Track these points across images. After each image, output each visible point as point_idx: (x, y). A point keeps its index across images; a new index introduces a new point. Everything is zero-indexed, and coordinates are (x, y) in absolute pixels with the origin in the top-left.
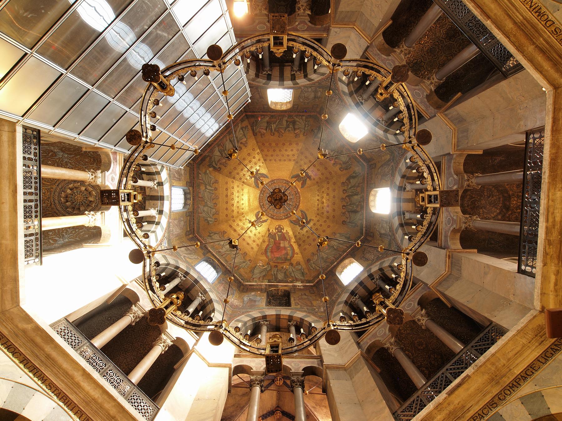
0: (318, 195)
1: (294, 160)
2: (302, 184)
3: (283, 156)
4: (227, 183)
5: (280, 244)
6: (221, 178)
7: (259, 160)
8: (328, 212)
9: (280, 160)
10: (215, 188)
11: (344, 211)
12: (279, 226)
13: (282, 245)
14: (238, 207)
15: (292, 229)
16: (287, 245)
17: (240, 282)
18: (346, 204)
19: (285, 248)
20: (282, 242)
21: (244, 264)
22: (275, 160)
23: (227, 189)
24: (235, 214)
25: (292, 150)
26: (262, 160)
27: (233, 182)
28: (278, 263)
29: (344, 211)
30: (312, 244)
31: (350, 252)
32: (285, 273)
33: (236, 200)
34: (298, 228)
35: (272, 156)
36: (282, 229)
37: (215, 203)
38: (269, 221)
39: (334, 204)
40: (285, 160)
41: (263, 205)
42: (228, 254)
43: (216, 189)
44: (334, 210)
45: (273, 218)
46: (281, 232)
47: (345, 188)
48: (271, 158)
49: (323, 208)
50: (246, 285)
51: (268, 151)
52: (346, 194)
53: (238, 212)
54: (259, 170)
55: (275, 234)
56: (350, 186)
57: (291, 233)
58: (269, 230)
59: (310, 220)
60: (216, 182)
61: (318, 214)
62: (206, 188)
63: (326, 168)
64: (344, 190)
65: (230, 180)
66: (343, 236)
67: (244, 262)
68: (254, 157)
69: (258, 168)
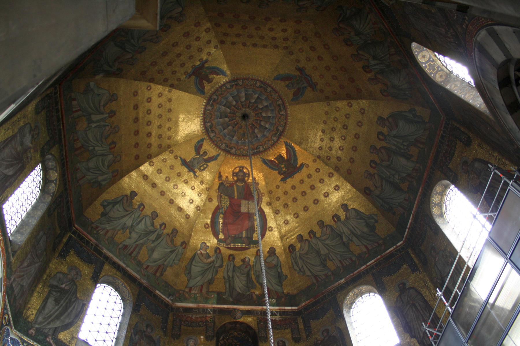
0: (325, 122)
1: (286, 48)
2: (295, 94)
3: (262, 38)
4: (136, 94)
5: (240, 206)
6: (123, 87)
7: (209, 42)
8: (339, 159)
9: (255, 45)
10: (112, 111)
11: (371, 171)
12: (241, 168)
13: (244, 209)
14: (160, 137)
15: (266, 177)
16: (253, 208)
17: (167, 305)
18: (378, 161)
19: (249, 216)
20: (244, 202)
21: (173, 256)
22: (244, 45)
23: (136, 107)
24: (154, 140)
25: (284, 31)
26: (215, 42)
27: (149, 88)
28: (235, 249)
29: (371, 171)
30: (301, 217)
31: (372, 267)
32: (248, 275)
33: (154, 130)
34: (277, 177)
35: (238, 35)
36: (245, 174)
37: (114, 143)
38: (220, 158)
39: (355, 149)
40: (265, 46)
41: (211, 127)
42: (143, 244)
43: (112, 114)
44: (352, 161)
45: (228, 152)
46: (243, 180)
47: (385, 130)
48: (235, 39)
49: (330, 149)
50: (178, 308)
51: (231, 26)
52: (384, 144)
53: (160, 146)
54: (207, 61)
55: (232, 185)
56: (394, 132)
57: (262, 183)
58: (220, 177)
59: (302, 165)
60: (113, 98)
61: (319, 157)
62: (90, 121)
63: (352, 80)
64: (380, 133)
65: (142, 85)
66: (361, 218)
67: (172, 252)
68: (198, 39)
69: (205, 57)
